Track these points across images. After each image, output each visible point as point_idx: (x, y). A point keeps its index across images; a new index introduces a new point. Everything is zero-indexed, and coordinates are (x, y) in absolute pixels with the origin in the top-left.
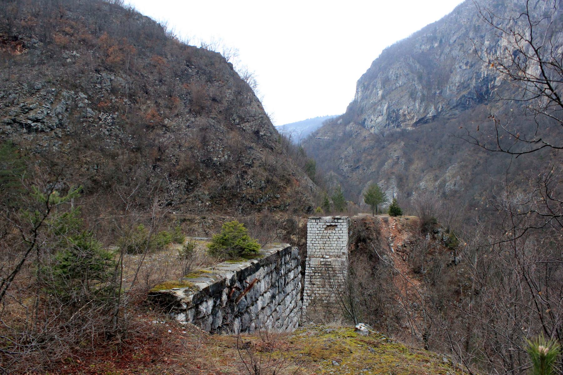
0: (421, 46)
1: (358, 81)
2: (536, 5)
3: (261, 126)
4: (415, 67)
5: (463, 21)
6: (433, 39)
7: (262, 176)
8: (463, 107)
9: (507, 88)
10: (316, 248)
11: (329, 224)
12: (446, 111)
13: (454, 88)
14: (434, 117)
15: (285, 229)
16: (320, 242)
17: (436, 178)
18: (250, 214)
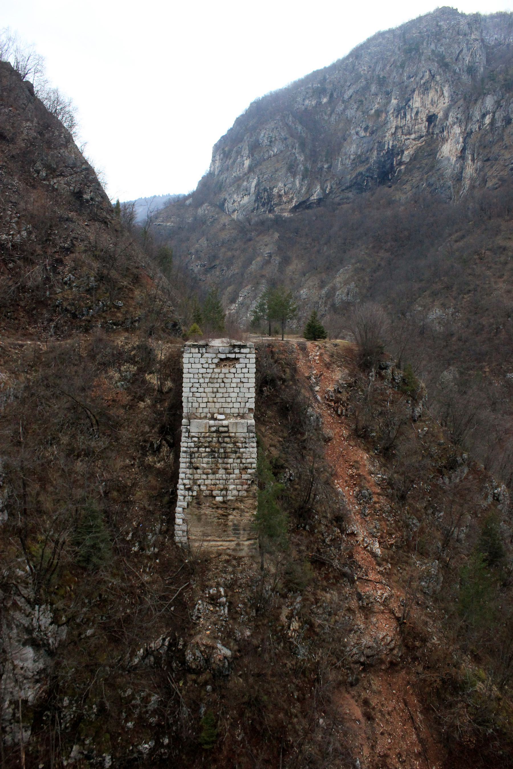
0: (304, 100)
1: (216, 145)
2: (458, 56)
3: (86, 184)
4: (296, 128)
5: (363, 69)
6: (320, 92)
7: (91, 268)
8: (359, 189)
9: (418, 166)
10: (200, 400)
11: (223, 356)
12: (336, 193)
13: (348, 162)
14: (320, 201)
15: (135, 363)
16: (207, 390)
17: (322, 284)
18: (70, 335)
